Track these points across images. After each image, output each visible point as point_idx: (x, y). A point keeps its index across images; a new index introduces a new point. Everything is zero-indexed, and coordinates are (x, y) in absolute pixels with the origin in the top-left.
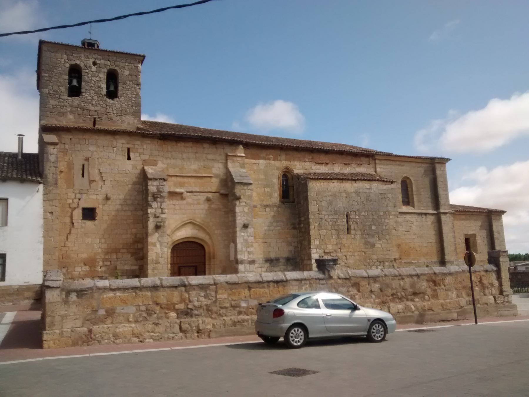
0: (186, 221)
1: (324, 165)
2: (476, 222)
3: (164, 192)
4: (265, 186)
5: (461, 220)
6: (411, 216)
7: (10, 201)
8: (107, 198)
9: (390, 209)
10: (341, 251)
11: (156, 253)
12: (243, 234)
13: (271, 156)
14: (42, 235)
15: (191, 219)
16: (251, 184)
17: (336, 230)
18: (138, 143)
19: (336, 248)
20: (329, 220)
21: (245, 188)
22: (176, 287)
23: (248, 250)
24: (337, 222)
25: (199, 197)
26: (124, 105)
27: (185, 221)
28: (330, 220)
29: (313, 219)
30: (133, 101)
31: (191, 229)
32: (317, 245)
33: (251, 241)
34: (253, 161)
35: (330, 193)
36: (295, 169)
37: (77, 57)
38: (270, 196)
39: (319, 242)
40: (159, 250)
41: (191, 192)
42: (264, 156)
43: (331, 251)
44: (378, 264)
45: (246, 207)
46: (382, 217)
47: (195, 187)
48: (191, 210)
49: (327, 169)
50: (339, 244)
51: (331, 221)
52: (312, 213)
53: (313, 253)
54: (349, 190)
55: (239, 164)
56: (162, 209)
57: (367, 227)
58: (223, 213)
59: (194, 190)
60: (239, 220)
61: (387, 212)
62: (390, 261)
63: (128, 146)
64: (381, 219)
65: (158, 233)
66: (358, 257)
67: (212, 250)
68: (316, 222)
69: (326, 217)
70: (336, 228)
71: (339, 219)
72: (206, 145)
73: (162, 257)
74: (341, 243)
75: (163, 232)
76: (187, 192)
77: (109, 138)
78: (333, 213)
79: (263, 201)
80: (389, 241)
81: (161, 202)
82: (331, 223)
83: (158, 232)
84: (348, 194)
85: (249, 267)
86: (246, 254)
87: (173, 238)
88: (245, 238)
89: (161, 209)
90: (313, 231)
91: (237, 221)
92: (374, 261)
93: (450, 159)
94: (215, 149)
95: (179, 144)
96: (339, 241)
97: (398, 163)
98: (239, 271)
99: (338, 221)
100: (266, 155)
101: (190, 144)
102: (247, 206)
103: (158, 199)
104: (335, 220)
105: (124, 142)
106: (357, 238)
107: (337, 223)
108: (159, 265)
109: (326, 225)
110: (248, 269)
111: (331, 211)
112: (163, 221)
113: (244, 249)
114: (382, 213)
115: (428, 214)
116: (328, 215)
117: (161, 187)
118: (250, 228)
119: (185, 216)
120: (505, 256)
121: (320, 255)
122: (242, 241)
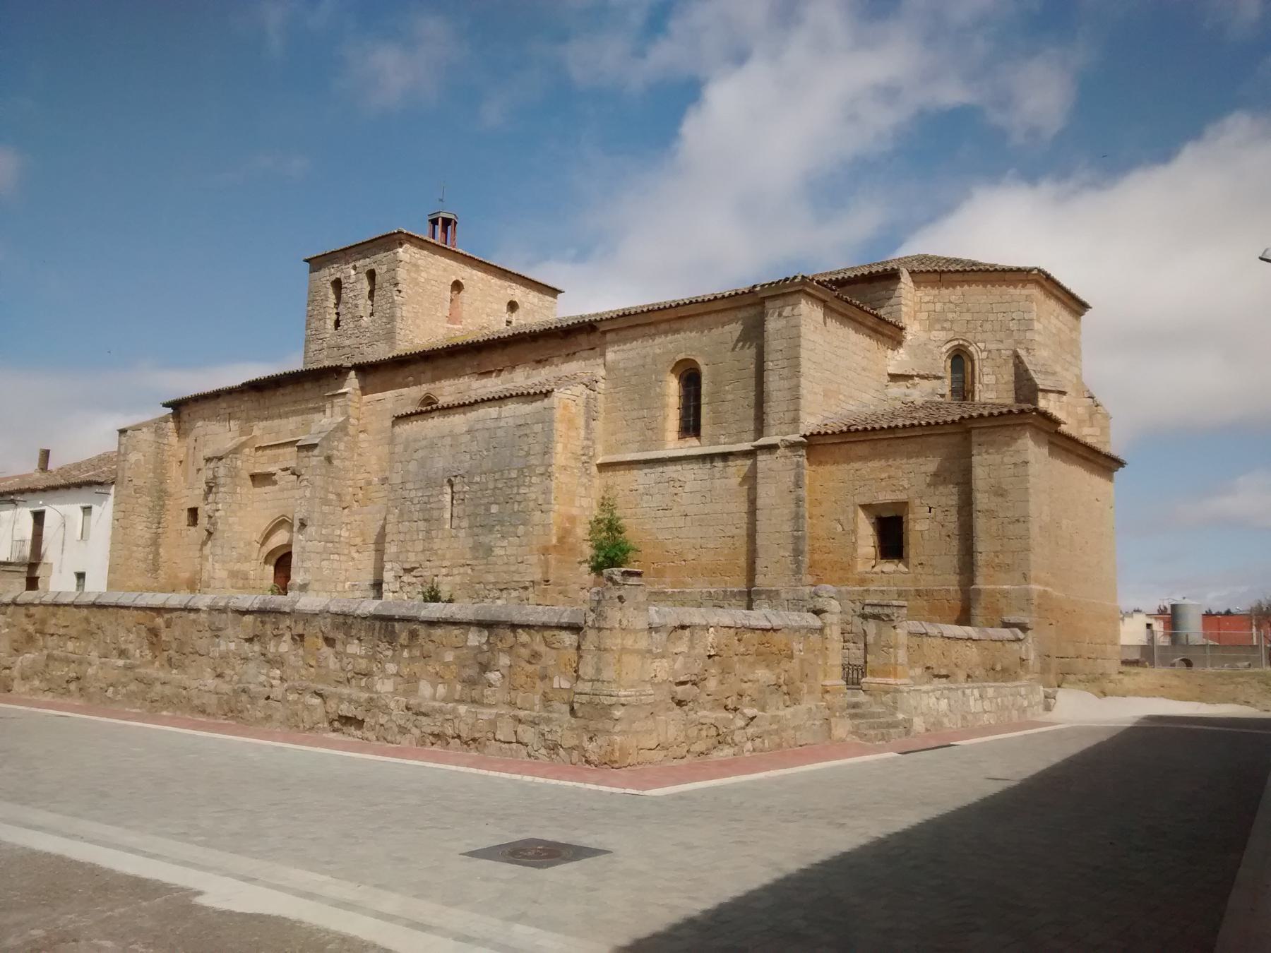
0: (279, 518)
1: (494, 374)
2: (913, 460)
5: (849, 460)
6: (679, 468)
7: (93, 509)
9: (534, 461)
12: (300, 537)
18: (237, 403)
19: (421, 557)
22: (338, 615)
35: (424, 443)
36: (442, 395)
43: (413, 566)
44: (497, 594)
46: (515, 483)
49: (499, 383)
54: (456, 431)
57: (481, 510)
61: (525, 470)
62: (522, 588)
63: (229, 411)
64: (512, 487)
66: (458, 579)
72: (308, 386)
74: (432, 548)
77: (212, 404)
79: (385, 471)
80: (525, 540)
84: (453, 435)
86: (302, 573)
88: (304, 542)
92: (488, 587)
97: (663, 327)
101: (289, 389)
103: (214, 489)
105: (224, 405)
106: (459, 535)
107: (429, 506)
113: (300, 564)
114: (514, 474)
115: (731, 454)
118: (310, 526)
119: (276, 510)
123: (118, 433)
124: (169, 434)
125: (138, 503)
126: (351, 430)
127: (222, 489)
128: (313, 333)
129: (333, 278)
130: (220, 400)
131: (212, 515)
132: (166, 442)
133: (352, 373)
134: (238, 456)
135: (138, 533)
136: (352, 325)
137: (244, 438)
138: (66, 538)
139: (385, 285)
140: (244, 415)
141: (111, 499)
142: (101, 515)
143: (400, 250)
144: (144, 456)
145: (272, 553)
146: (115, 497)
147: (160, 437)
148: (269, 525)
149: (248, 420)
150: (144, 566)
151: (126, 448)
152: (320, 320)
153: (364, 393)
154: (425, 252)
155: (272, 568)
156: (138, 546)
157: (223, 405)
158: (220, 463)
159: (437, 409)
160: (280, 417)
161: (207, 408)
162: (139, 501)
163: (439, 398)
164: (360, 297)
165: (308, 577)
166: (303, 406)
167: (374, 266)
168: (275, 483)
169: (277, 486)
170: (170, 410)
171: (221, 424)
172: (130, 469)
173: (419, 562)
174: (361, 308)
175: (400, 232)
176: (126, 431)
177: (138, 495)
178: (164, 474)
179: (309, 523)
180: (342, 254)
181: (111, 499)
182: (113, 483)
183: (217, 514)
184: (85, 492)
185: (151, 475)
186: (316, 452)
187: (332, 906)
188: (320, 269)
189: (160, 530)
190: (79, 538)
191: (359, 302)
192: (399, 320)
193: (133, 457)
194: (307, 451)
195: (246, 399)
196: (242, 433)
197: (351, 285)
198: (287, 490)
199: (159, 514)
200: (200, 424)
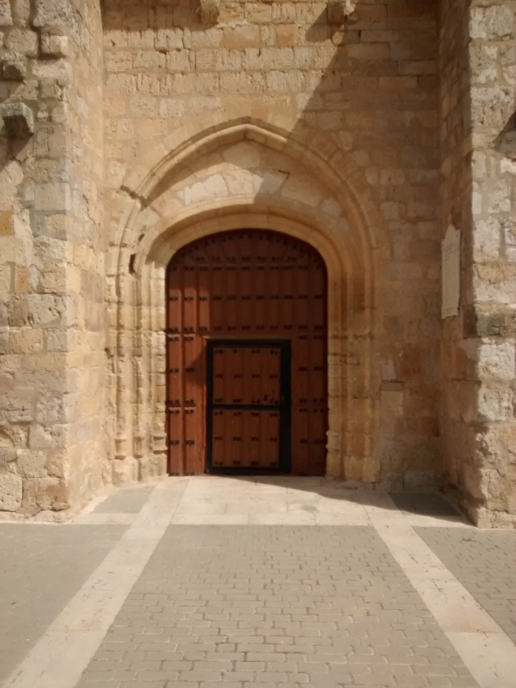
0: (223, 126)
11: (12, 264)
27: (214, 129)
31: (253, 170)
40: (29, 251)
48: (250, 72)
56: (37, 30)
58: (413, 83)
60: (488, 84)
65: (21, 163)
67: (349, 270)
73: (41, 292)
75: (47, 157)
83: (20, 156)
87: (167, 212)
89: (32, 36)
91: (476, 94)
93: (236, 671)
98: (481, 374)
108: (27, 328)
119: (217, 102)
148: (185, 145)
155: (162, 273)
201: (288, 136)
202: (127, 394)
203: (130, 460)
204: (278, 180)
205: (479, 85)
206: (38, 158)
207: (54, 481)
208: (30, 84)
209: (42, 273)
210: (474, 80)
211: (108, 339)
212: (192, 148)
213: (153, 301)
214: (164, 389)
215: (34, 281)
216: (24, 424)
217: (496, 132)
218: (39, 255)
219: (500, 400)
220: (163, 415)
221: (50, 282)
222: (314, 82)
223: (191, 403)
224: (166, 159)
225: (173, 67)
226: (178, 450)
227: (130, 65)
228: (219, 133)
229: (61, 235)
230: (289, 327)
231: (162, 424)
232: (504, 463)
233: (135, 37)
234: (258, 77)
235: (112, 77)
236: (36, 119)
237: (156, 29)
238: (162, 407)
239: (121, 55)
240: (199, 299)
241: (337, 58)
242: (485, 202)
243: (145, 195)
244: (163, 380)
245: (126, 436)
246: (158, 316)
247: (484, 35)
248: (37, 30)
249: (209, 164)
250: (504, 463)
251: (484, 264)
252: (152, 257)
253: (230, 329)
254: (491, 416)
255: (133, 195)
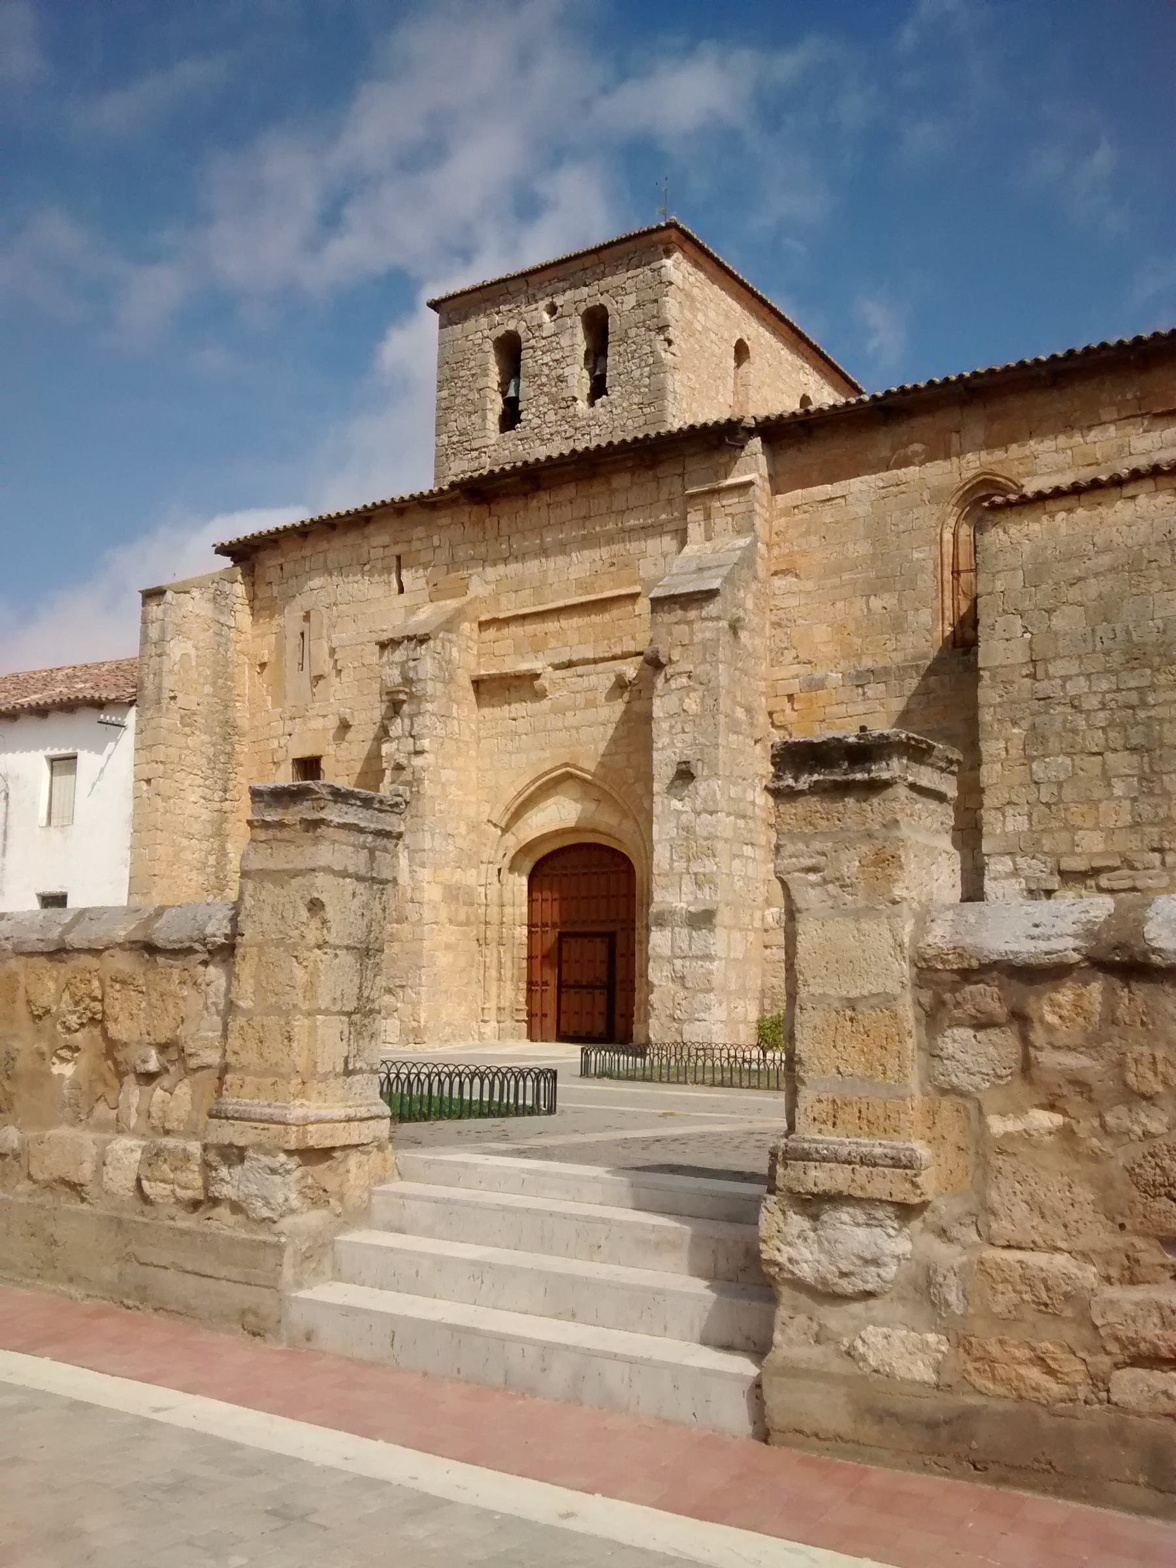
0: (552, 770)
3: (420, 680)
4: (873, 590)
8: (345, 726)
10: (1163, 863)
12: (676, 804)
13: (917, 447)
14: (128, 844)
15: (567, 765)
16: (711, 594)
17: (1134, 750)
18: (419, 532)
20: (1093, 702)
21: (692, 614)
23: (696, 867)
24: (1144, 704)
25: (593, 679)
26: (619, 410)
27: (546, 773)
28: (1099, 697)
29: (1000, 705)
30: (643, 390)
31: (576, 800)
32: (1018, 834)
33: (705, 834)
34: (828, 489)
35: (1106, 560)
37: (510, 311)
38: (897, 625)
39: (1030, 816)
41: (570, 665)
42: (885, 453)
43: (1098, 863)
45: (692, 695)
47: (580, 643)
48: (567, 729)
50: (1152, 824)
51: (1104, 706)
52: (993, 677)
53: (995, 879)
55: (730, 519)
59: (575, 658)
60: (663, 749)
63: (397, 550)
68: (1015, 723)
69: (1072, 689)
70: (1137, 737)
71: (1153, 687)
72: (621, 481)
76: (557, 667)
77: (352, 538)
78: (1122, 660)
79: (859, 656)
81: (411, 717)
82: (1101, 718)
85: (691, 937)
86: (688, 885)
87: (521, 836)
89: (411, 740)
90: (998, 767)
91: (655, 755)
94: (652, 486)
95: (534, 503)
96: (1156, 806)
99: (1151, 700)
100: (894, 449)
102: (695, 690)
103: (405, 707)
104: (1133, 697)
105: (385, 539)
107: (1142, 714)
109: (1075, 731)
110: (685, 946)
111: (1107, 653)
112: (416, 780)
113: (680, 866)
116: (1088, 676)
117: (411, 664)
118: (706, 779)
119: (547, 754)
120: (286, 834)
121: (1033, 887)
122: (674, 833)
123: (140, 595)
124: (238, 607)
125: (187, 747)
126: (761, 570)
127: (429, 706)
128: (455, 439)
129: (500, 332)
130: (371, 528)
131: (404, 761)
132: (232, 623)
133: (756, 443)
134: (453, 637)
135: (190, 810)
136: (550, 416)
137: (452, 604)
138: (10, 823)
139: (633, 332)
140: (443, 555)
141: (128, 738)
142: (102, 770)
143: (668, 262)
144: (197, 649)
145: (526, 849)
146: (140, 732)
147: (222, 612)
148: (528, 786)
149: (453, 564)
150: (201, 879)
151: (163, 630)
152: (470, 414)
153: (776, 491)
154: (702, 275)
155: (524, 880)
156: (190, 836)
157: (379, 540)
158: (422, 650)
159: (1009, 505)
160: (544, 552)
161: (338, 548)
162: (191, 742)
163: (1024, 481)
164: (569, 360)
165: (905, 893)
166: (611, 526)
167: (603, 300)
168: (540, 695)
169: (545, 704)
170: (227, 562)
171: (376, 578)
172: (171, 671)
173: (1120, 854)
174: (573, 381)
175: (672, 226)
176: (165, 592)
177: (187, 730)
178: (230, 689)
179: (699, 770)
180: (521, 283)
181: (128, 738)
182: (131, 704)
183: (417, 761)
184: (57, 724)
185: (208, 689)
186: (712, 609)
187: (450, 1502)
188: (466, 318)
189: (227, 805)
190: (44, 822)
191: (567, 371)
192: (670, 397)
193: (177, 649)
194: (684, 608)
195: (445, 521)
196: (436, 593)
197: (544, 342)
198: (574, 708)
199: (224, 771)
200: (316, 582)
201: (593, 775)
202: (493, 973)
203: (494, 1024)
204: (592, 806)
205: (658, 749)
206: (412, 817)
207: (415, 1024)
208: (409, 770)
209: (413, 889)
210: (655, 745)
211: (478, 932)
212: (532, 788)
213: (517, 902)
214: (525, 971)
215: (409, 896)
216: (402, 987)
217: (668, 782)
218: (412, 878)
219: (662, 971)
220: (524, 992)
221: (417, 896)
222: (610, 732)
223: (545, 983)
224: (516, 798)
225: (520, 731)
226: (536, 1021)
227: (494, 731)
228: (549, 776)
229: (423, 865)
230: (613, 921)
231: (522, 999)
232: (663, 1016)
233: (497, 710)
234: (574, 731)
235: (483, 741)
236: (411, 792)
237: (509, 704)
238: (523, 986)
239: (488, 724)
240: (553, 900)
241: (625, 712)
242: (660, 832)
243: (503, 825)
244: (524, 964)
245: (492, 1004)
246: (521, 914)
247: (661, 715)
248: (413, 737)
249: (548, 797)
250: (663, 1016)
251: (659, 875)
252: (512, 869)
253: (574, 923)
254: (656, 982)
255: (495, 825)
